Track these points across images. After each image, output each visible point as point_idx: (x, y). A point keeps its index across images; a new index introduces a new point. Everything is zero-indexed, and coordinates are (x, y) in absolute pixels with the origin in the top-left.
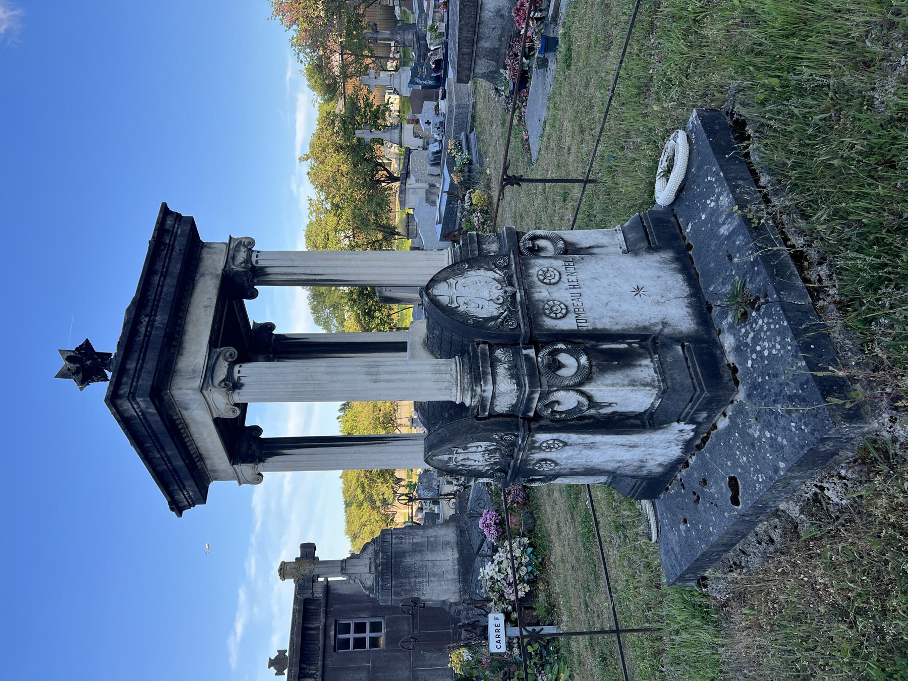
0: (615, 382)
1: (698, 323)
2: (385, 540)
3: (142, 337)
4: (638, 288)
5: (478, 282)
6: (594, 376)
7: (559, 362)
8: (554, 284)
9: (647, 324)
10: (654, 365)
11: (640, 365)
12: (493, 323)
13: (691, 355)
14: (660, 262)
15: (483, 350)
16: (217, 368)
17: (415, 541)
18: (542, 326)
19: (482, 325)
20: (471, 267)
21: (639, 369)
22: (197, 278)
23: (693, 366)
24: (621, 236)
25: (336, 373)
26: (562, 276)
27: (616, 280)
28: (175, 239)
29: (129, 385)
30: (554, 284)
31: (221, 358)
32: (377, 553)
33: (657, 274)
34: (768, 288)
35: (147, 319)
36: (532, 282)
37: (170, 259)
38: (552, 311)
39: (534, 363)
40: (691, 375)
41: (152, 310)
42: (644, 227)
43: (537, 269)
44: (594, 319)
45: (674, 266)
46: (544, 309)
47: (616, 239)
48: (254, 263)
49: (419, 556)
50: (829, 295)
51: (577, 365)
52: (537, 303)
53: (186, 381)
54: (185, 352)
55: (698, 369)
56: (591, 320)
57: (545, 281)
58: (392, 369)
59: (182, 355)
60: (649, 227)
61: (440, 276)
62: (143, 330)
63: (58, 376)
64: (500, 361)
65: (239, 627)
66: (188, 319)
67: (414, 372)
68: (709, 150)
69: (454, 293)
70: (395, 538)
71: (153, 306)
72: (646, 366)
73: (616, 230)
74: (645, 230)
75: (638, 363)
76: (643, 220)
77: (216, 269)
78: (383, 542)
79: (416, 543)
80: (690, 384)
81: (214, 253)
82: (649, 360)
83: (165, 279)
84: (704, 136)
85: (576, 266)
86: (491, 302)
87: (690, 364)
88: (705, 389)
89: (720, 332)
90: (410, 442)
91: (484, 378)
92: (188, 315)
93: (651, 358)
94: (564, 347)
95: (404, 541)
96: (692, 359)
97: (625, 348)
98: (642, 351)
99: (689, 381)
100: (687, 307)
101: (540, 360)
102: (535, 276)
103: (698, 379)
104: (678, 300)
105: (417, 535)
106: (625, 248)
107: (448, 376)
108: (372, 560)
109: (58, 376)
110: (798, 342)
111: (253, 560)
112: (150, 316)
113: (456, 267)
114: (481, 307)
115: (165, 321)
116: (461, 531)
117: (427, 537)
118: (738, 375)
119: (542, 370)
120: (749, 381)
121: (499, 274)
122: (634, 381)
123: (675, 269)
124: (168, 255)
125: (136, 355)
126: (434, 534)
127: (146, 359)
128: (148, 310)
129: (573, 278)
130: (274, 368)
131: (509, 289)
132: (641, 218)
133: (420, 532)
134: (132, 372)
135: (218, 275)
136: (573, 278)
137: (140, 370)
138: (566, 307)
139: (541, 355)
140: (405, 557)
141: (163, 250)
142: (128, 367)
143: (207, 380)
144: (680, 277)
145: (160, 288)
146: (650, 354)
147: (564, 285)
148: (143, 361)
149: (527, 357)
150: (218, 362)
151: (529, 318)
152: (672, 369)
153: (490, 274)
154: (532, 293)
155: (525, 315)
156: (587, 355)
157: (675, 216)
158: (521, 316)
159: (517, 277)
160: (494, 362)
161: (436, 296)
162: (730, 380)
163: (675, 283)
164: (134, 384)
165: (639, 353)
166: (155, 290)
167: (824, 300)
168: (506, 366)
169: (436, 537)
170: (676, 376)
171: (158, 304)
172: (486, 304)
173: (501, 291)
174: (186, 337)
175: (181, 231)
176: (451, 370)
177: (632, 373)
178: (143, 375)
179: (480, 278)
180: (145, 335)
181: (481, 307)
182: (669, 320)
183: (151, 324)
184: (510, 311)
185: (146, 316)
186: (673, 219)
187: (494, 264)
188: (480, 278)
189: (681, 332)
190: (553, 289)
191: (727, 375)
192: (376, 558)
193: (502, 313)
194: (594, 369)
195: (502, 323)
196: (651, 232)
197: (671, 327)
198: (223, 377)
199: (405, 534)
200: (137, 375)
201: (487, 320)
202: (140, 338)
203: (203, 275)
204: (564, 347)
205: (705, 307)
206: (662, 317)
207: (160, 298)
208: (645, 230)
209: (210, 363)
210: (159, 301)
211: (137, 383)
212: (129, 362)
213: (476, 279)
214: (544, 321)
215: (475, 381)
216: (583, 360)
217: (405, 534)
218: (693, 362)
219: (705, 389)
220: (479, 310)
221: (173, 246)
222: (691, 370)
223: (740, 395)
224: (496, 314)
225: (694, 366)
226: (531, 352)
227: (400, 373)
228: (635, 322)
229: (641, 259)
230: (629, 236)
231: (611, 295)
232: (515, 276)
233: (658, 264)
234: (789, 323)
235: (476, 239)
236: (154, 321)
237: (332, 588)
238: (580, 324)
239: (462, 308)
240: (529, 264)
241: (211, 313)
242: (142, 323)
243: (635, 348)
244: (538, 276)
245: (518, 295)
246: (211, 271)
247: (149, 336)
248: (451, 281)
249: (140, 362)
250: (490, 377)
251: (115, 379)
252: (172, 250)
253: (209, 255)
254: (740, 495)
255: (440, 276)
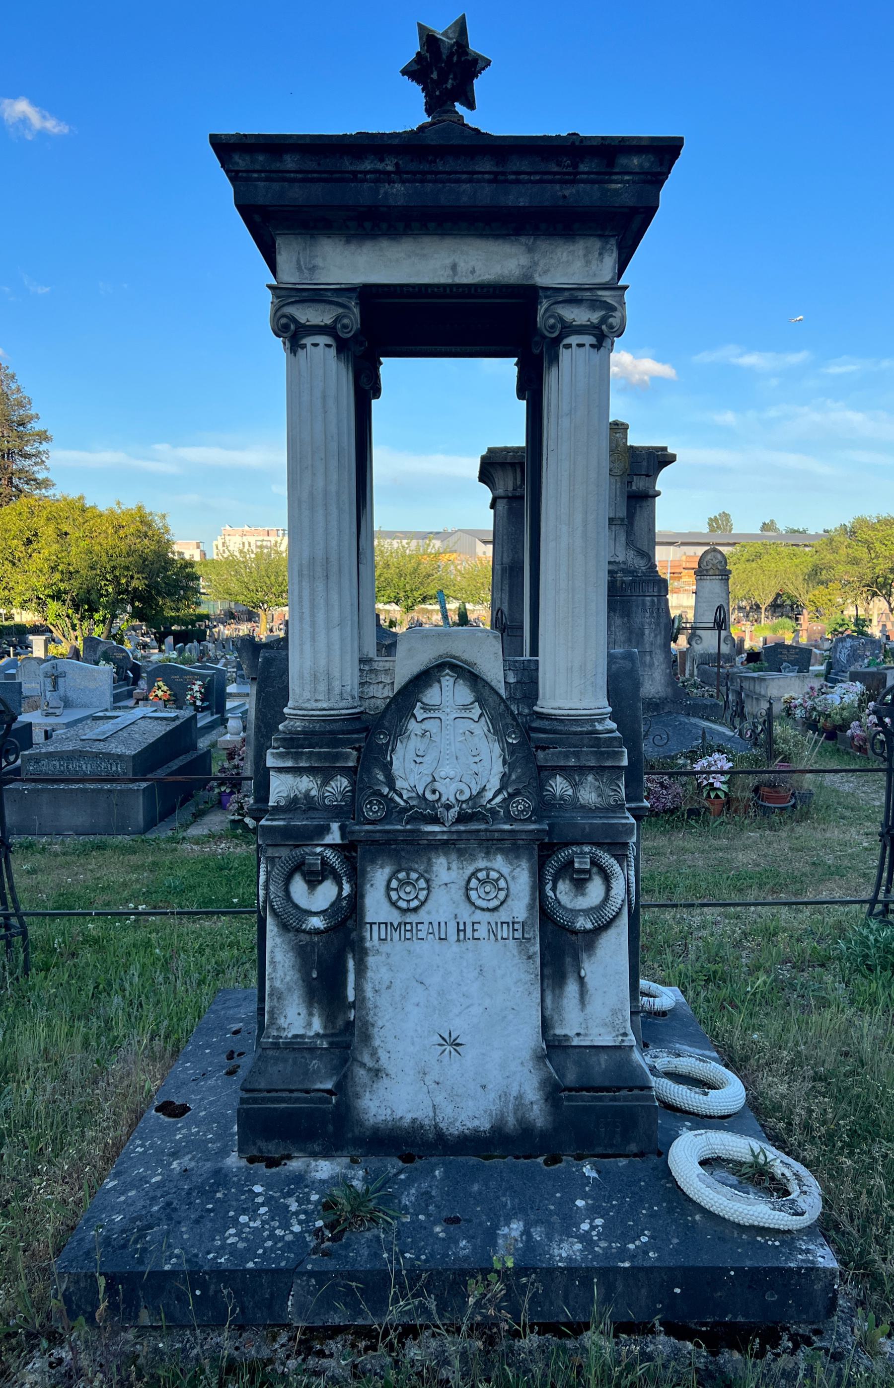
0: (279, 967)
1: (378, 1129)
2: (651, 585)
3: (351, 168)
4: (458, 1045)
5: (477, 759)
6: (291, 935)
7: (320, 882)
8: (468, 898)
9: (377, 1043)
10: (310, 1037)
11: (311, 1014)
12: (381, 777)
13: (311, 1101)
14: (519, 1097)
15: (347, 757)
16: (321, 307)
17: (647, 632)
18: (373, 861)
19: (376, 759)
20: (512, 749)
21: (304, 1012)
22: (523, 239)
23: (306, 1098)
24: (607, 1040)
25: (312, 509)
26: (487, 914)
27: (476, 1010)
28: (593, 182)
29: (251, 168)
30: (468, 898)
31: (340, 310)
32: (632, 572)
33: (490, 1086)
34: (334, 1262)
35: (390, 168)
36: (473, 858)
37: (540, 181)
38: (403, 883)
39: (312, 840)
40: (277, 1091)
41: (414, 173)
42: (619, 1089)
43: (505, 871)
44: (388, 955)
45: (511, 1121)
46: (408, 870)
47: (602, 1031)
48: (566, 341)
49: (623, 639)
50: (288, 1357)
51: (313, 910)
52: (425, 859)
53: (294, 259)
54: (353, 247)
55: (283, 1105)
56: (385, 948)
57: (474, 880)
58: (321, 602)
59: (348, 242)
60: (614, 1099)
61: (486, 692)
62: (367, 166)
63: (419, 25)
64: (325, 783)
65: (751, 360)
66: (426, 240)
67: (313, 639)
68: (704, 1260)
69: (449, 714)
70: (653, 601)
71: (424, 173)
72: (309, 1024)
73: (625, 1034)
74: (601, 1089)
75: (315, 1011)
76: (636, 1092)
77: (546, 272)
78: (648, 582)
79: (643, 634)
80: (257, 1086)
81: (588, 263)
82: (321, 1032)
83: (490, 182)
84: (748, 1264)
85: (511, 943)
86: (430, 779)
87: (295, 1095)
88: (245, 1106)
89: (354, 1161)
90: (356, 631)
91: (288, 753)
92: (436, 238)
93: (324, 1036)
94: (345, 893)
95: (648, 615)
96: (305, 1101)
97: (346, 997)
98: (340, 1023)
99: (262, 1086)
100: (414, 1120)
101: (319, 850)
102: (489, 864)
103: (264, 1100)
104: (430, 1110)
105: (656, 636)
106: (574, 1043)
107: (307, 695)
108: (622, 566)
109: (419, 25)
110: (205, 1273)
111: (851, 368)
112: (398, 171)
113: (509, 720)
114: (419, 760)
115: (391, 202)
116: (657, 705)
117: (651, 652)
118: (262, 1165)
119: (299, 851)
120: (235, 1179)
121: (492, 797)
122: (279, 998)
123: (502, 1118)
124: (550, 177)
125: (312, 165)
126: (656, 663)
127: (308, 185)
128: (413, 166)
129: (482, 931)
130: (324, 406)
131: (453, 813)
132: (642, 1088)
133: (660, 641)
134: (277, 166)
135: (531, 277)
136: (482, 931)
137: (285, 180)
138: (415, 910)
139: (328, 853)
140: (622, 617)
141: (558, 165)
142: (287, 158)
143: (294, 293)
144: (485, 1125)
145: (464, 176)
146: (332, 1035)
147: (466, 914)
148: (303, 180)
149: (326, 829)
150: (333, 307)
151: (388, 843)
152: (295, 1063)
153: (494, 783)
154: (446, 854)
155: (391, 836)
156: (327, 930)
157: (641, 1154)
158: (388, 827)
159: (478, 831)
160: (325, 774)
161: (439, 682)
162: (260, 1150)
163: (470, 1114)
164: (255, 175)
165: (336, 1018)
166: (458, 169)
167: (283, 1345)
168: (313, 793)
169: (651, 665)
170: (281, 1067)
171: (429, 181)
172: (426, 769)
173: (452, 799)
174: (385, 243)
175: (616, 190)
176: (316, 701)
177: (295, 996)
178: (276, 186)
179: (486, 763)
180: (355, 173)
181: (419, 760)
182: (385, 1081)
183: (384, 177)
184: (405, 810)
185: (397, 165)
186: (633, 1148)
187: (517, 793)
188: (486, 763)
189: (357, 1096)
190: (457, 893)
191: (272, 1149)
192: (626, 572)
193: (401, 796)
194: (303, 936)
195: (379, 794)
196: (600, 1099)
197: (369, 1083)
198: (303, 320)
199: (658, 617)
200: (274, 175)
201: (387, 768)
202: (348, 165)
203: (530, 250)
204: (345, 893)
205: (415, 1151)
206: (391, 1070)
207: (442, 182)
208: (608, 1090)
209: (329, 294)
210: (435, 181)
211: (258, 179)
212: (297, 157)
213: (485, 755)
214: (382, 867)
215: (284, 739)
216: (317, 922)
217: (658, 617)
218: (297, 1100)
219: (245, 1106)
220: (411, 755)
221: (573, 182)
222: (285, 1094)
223: (234, 1161)
224: (399, 784)
225: (305, 1101)
226: (334, 836)
227: (313, 615)
228: (380, 1024)
229: (530, 1065)
230: (604, 1057)
231: (441, 993)
232: (483, 827)
233: (514, 1093)
234: (250, 1271)
235: (608, 764)
236: (391, 182)
237: (645, 504)
238: (375, 927)
239: (413, 726)
240: (518, 857)
241: (443, 277)
242: (382, 160)
243: (345, 1013)
244: (488, 869)
245: (436, 828)
246: (541, 263)
247: (355, 179)
248: (476, 711)
249: (300, 176)
250: (289, 764)
251: (253, 141)
252: (565, 182)
253: (581, 253)
254: (162, 1116)
255: (486, 692)
